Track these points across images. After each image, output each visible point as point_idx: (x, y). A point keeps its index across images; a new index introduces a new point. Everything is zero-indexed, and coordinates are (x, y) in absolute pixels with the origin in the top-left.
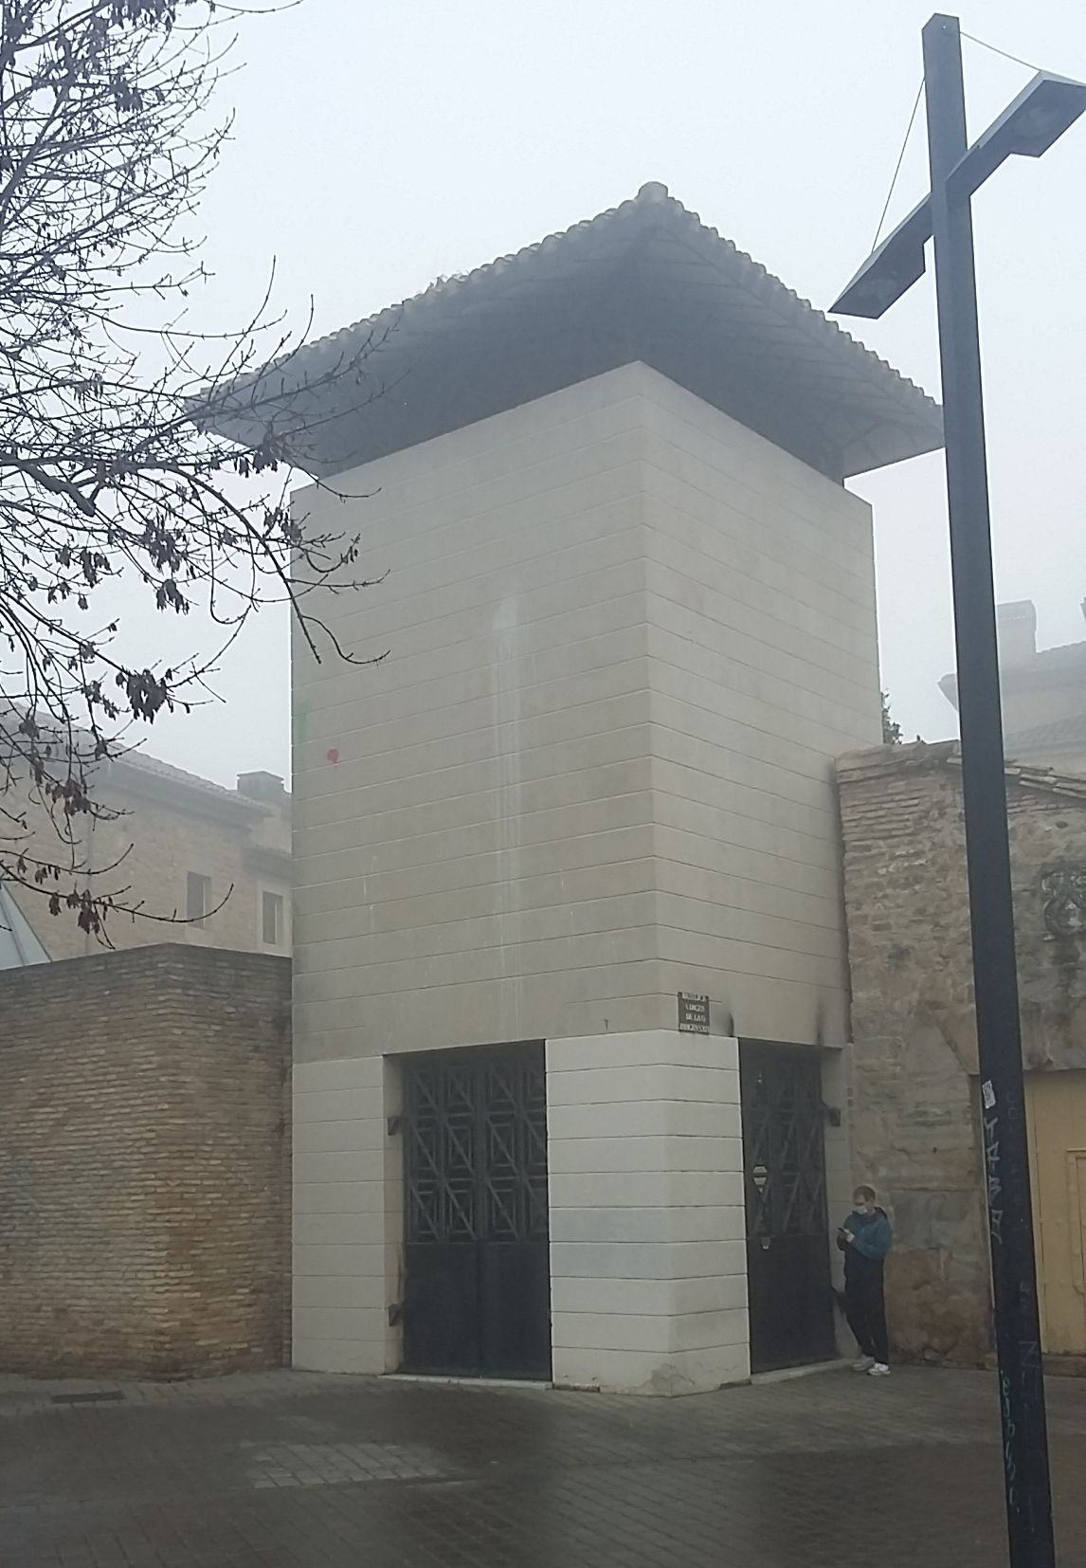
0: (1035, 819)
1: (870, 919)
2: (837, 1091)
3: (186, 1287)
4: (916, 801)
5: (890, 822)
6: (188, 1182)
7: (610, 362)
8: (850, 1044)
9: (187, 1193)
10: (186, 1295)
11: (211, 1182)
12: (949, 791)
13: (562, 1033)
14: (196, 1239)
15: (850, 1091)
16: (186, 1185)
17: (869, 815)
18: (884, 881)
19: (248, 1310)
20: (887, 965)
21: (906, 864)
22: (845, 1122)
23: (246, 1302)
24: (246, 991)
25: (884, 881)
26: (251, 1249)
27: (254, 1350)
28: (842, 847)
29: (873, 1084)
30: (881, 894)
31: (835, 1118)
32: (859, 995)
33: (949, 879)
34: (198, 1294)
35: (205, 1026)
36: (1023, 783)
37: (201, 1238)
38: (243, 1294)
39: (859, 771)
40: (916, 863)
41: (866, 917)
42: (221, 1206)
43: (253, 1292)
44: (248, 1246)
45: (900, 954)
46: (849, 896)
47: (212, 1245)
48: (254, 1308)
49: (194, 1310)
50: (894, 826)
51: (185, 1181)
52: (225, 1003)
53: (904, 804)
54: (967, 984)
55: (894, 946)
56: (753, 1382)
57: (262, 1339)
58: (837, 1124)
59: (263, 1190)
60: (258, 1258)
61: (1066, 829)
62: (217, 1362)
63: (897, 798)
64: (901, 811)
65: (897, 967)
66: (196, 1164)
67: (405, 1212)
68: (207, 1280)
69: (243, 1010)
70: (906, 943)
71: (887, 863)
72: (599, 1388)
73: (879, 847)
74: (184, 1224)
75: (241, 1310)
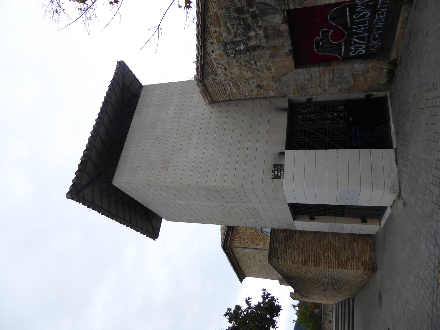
0: (212, 58)
1: (249, 93)
2: (302, 99)
3: (353, 264)
4: (214, 85)
5: (221, 90)
6: (326, 261)
7: (118, 191)
8: (287, 96)
9: (329, 261)
10: (355, 264)
11: (326, 254)
12: (209, 78)
13: (286, 200)
14: (340, 260)
15: (302, 96)
16: (327, 261)
17: (220, 95)
18: (238, 91)
19: (359, 243)
20: (263, 89)
21: (232, 86)
22: (311, 97)
23: (357, 244)
24: (279, 239)
25: (238, 91)
26: (344, 242)
27: (370, 242)
28: (230, 100)
29: (299, 91)
30: (242, 91)
31: (309, 100)
32: (272, 95)
33: (234, 77)
34: (355, 260)
35: (288, 253)
36: (202, 63)
37: (340, 258)
38: (355, 245)
39: (208, 99)
40: (231, 84)
41: (249, 94)
42: (332, 251)
43: (355, 242)
44: (343, 243)
45: (259, 86)
46: (243, 98)
47: (342, 254)
48: (359, 242)
49: (359, 261)
50: (222, 89)
51: (326, 262)
52: (282, 246)
53: (215, 88)
54: (266, 71)
55: (257, 88)
56: (396, 148)
57: (367, 239)
58: (312, 99)
59: (328, 236)
60: (346, 240)
61: (214, 51)
62: (373, 255)
63: (214, 89)
64: (217, 88)
65: (263, 87)
66: (321, 258)
67: (336, 101)
68: (351, 257)
69: (284, 240)
70: (255, 85)
71: (233, 90)
72: (394, 201)
73: (228, 92)
74: (336, 263)
75: (359, 246)
